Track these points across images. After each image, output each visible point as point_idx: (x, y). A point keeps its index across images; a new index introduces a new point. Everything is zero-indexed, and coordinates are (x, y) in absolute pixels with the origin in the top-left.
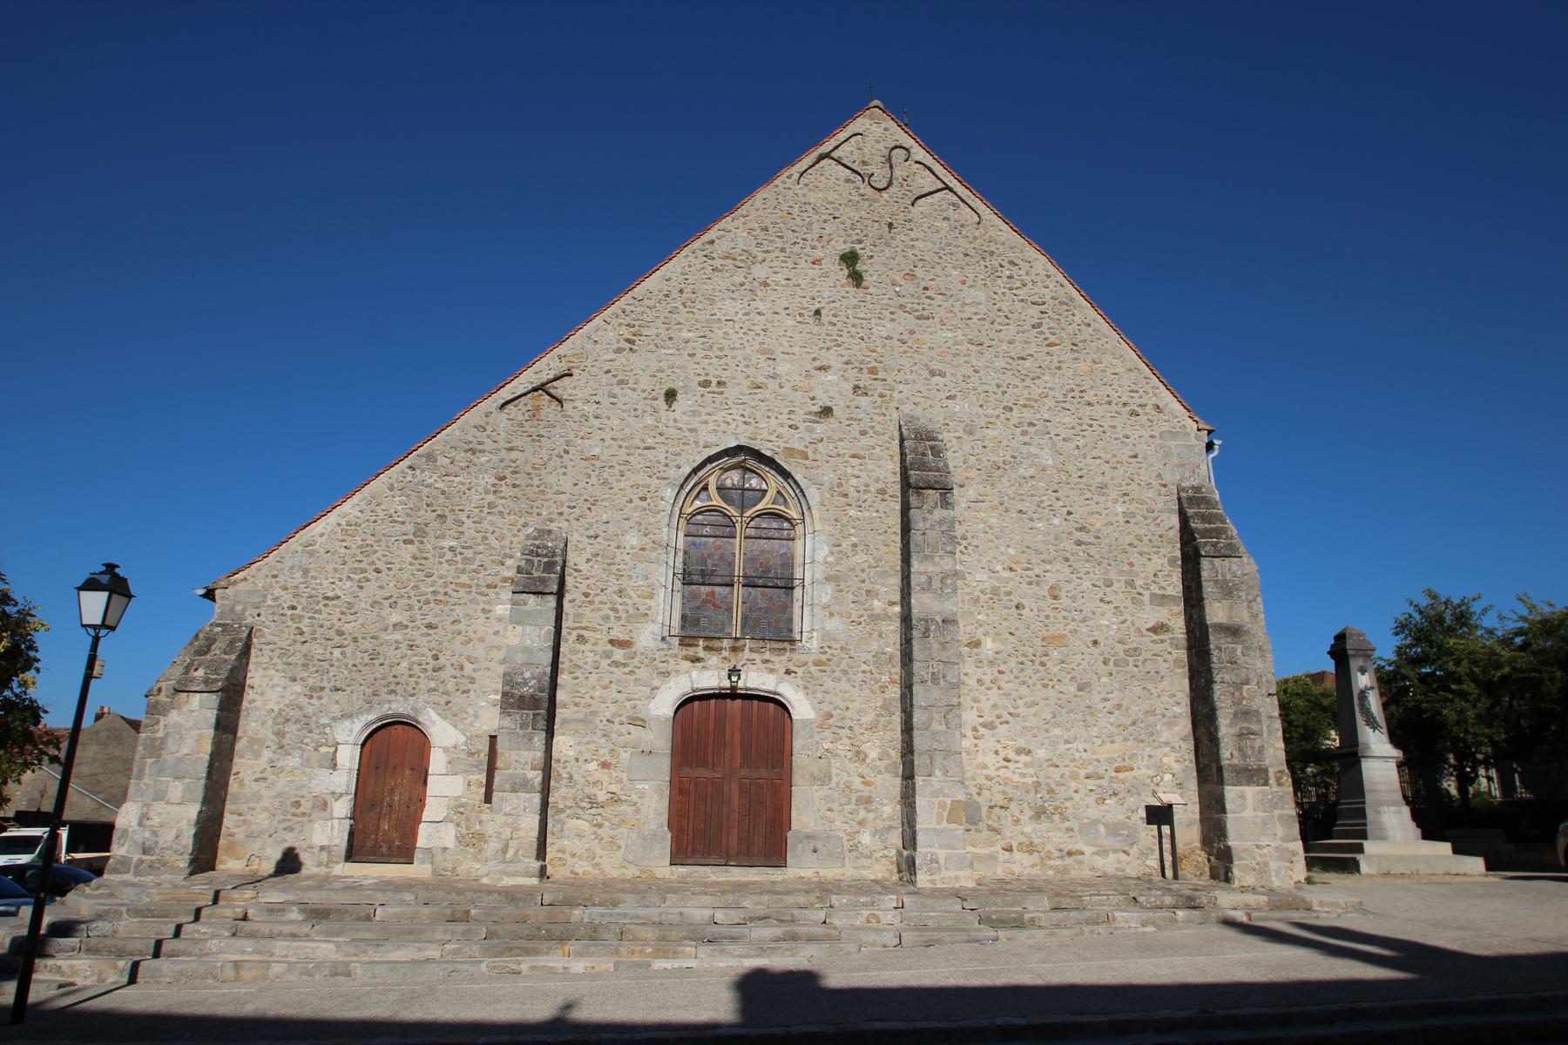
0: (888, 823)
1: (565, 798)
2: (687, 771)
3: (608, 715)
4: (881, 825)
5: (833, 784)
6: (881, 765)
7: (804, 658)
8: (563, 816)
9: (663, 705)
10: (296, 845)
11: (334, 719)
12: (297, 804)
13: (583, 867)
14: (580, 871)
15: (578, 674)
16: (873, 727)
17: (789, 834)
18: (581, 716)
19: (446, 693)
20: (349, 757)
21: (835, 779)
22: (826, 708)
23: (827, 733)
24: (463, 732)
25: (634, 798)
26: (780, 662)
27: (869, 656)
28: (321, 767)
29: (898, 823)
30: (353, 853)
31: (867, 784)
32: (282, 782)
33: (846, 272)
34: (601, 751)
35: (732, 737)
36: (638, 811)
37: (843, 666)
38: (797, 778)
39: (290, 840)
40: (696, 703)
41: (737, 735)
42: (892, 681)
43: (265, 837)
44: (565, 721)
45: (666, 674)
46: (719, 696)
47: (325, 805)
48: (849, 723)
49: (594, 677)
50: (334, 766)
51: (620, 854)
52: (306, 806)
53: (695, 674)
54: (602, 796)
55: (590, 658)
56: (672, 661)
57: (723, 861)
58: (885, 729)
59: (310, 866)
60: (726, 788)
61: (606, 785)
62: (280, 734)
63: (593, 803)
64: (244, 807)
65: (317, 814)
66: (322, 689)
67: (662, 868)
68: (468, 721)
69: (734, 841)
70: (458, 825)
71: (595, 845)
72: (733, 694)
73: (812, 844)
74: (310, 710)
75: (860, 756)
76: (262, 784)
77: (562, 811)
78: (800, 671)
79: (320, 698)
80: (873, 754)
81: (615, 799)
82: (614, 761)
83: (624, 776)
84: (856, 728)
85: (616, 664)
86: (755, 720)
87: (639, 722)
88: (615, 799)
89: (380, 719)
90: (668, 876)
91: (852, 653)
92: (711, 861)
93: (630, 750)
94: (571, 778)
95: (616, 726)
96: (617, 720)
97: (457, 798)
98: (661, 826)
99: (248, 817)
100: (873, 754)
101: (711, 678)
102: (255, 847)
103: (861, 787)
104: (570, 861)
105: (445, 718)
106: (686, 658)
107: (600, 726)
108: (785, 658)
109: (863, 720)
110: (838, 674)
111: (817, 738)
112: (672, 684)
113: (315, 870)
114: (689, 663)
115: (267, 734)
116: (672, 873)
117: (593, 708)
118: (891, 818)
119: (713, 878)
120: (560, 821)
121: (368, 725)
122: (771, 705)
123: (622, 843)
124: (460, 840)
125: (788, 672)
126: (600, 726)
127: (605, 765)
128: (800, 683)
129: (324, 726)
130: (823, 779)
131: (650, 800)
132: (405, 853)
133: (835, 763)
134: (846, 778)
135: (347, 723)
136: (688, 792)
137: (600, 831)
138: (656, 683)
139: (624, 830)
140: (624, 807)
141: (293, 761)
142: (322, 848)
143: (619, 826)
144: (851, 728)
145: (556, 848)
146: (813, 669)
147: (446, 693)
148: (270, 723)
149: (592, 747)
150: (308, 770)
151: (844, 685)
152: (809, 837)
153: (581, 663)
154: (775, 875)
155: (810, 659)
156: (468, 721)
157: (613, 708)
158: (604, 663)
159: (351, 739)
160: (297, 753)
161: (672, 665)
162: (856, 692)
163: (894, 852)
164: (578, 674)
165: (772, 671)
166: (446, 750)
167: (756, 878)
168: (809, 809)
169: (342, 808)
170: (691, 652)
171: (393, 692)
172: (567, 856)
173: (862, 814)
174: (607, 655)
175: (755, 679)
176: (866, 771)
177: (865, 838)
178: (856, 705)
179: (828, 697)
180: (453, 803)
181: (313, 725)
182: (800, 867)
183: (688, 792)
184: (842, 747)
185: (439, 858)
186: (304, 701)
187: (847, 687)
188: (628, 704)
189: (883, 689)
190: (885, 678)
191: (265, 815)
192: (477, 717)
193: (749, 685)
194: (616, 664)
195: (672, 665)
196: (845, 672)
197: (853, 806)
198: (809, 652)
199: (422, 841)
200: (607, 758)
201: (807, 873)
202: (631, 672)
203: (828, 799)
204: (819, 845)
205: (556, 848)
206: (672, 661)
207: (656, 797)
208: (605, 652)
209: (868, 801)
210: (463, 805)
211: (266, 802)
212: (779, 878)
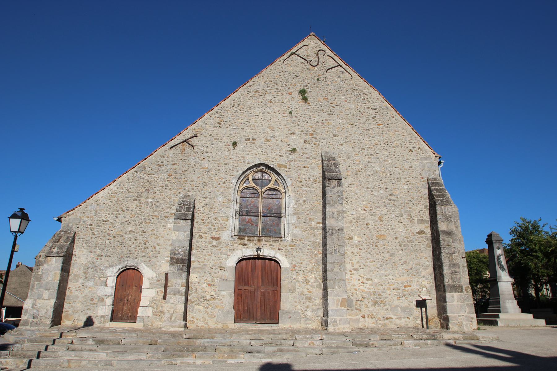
0: (317, 307)
1: (194, 298)
4: (315, 308)
5: (297, 292)
6: (315, 285)
7: (286, 244)
8: (193, 304)
9: (232, 262)
10: (92, 315)
11: (106, 267)
12: (92, 300)
13: (201, 324)
14: (200, 325)
15: (199, 250)
16: (312, 270)
17: (280, 311)
18: (200, 266)
19: (149, 257)
20: (112, 281)
22: (294, 263)
23: (294, 273)
24: (155, 272)
25: (221, 297)
26: (276, 245)
27: (310, 243)
28: (101, 285)
30: (112, 319)
31: (310, 292)
32: (86, 291)
33: (301, 97)
34: (208, 280)
36: (222, 303)
37: (300, 247)
39: (90, 313)
40: (244, 261)
41: (260, 274)
42: (319, 253)
43: (80, 312)
44: (194, 268)
45: (233, 250)
47: (103, 300)
48: (303, 269)
49: (205, 251)
50: (106, 285)
51: (215, 319)
52: (95, 300)
53: (244, 250)
54: (208, 297)
56: (235, 245)
57: (254, 322)
58: (316, 271)
59: (97, 323)
60: (256, 294)
61: (210, 292)
62: (86, 273)
63: (205, 299)
64: (72, 301)
65: (100, 303)
66: (102, 256)
67: (231, 324)
68: (157, 268)
70: (153, 308)
71: (206, 316)
72: (258, 258)
74: (97, 264)
75: (307, 281)
76: (79, 292)
77: (193, 302)
78: (284, 249)
79: (101, 259)
80: (312, 281)
81: (213, 298)
82: (213, 283)
83: (217, 289)
84: (305, 271)
85: (214, 246)
86: (267, 268)
87: (222, 268)
88: (213, 298)
89: (124, 267)
90: (233, 327)
91: (304, 242)
92: (250, 322)
93: (219, 279)
94: (196, 290)
95: (214, 270)
96: (214, 268)
97: (153, 298)
99: (73, 305)
100: (312, 281)
101: (250, 251)
102: (76, 316)
103: (307, 293)
104: (196, 321)
105: (148, 267)
106: (240, 244)
107: (208, 270)
109: (308, 267)
110: (298, 250)
111: (290, 274)
112: (235, 254)
113: (99, 325)
114: (242, 246)
115: (81, 273)
117: (205, 263)
118: (319, 305)
119: (251, 328)
120: (192, 306)
121: (119, 269)
122: (273, 262)
123: (216, 315)
124: (154, 313)
125: (279, 249)
126: (208, 270)
127: (209, 285)
128: (284, 253)
129: (103, 270)
130: (293, 290)
131: (227, 298)
132: (133, 318)
133: (297, 284)
135: (111, 269)
137: (207, 310)
138: (229, 253)
140: (217, 301)
141: (91, 283)
142: (102, 317)
143: (215, 308)
144: (303, 271)
145: (191, 316)
146: (289, 248)
147: (149, 257)
148: (82, 268)
149: (204, 278)
150: (96, 287)
151: (301, 254)
153: (200, 246)
154: (274, 327)
155: (288, 244)
156: (157, 268)
158: (209, 246)
159: (113, 275)
160: (92, 280)
162: (305, 257)
163: (320, 318)
164: (199, 250)
165: (273, 249)
166: (149, 279)
167: (267, 328)
168: (287, 301)
169: (109, 301)
170: (242, 241)
171: (129, 257)
172: (195, 320)
173: (308, 303)
174: (210, 243)
175: (267, 252)
176: (309, 287)
177: (309, 313)
178: (305, 262)
179: (295, 259)
180: (151, 299)
181: (98, 270)
182: (284, 324)
183: (241, 295)
184: (300, 278)
185: (146, 320)
186: (95, 260)
187: (302, 255)
188: (218, 261)
189: (316, 256)
190: (316, 252)
191: (80, 304)
192: (161, 266)
193: (265, 254)
194: (214, 246)
196: (301, 249)
197: (304, 300)
199: (139, 314)
200: (210, 282)
202: (220, 249)
204: (291, 316)
205: (191, 316)
206: (235, 245)
207: (229, 297)
209: (310, 298)
210: (155, 300)
211: (80, 299)
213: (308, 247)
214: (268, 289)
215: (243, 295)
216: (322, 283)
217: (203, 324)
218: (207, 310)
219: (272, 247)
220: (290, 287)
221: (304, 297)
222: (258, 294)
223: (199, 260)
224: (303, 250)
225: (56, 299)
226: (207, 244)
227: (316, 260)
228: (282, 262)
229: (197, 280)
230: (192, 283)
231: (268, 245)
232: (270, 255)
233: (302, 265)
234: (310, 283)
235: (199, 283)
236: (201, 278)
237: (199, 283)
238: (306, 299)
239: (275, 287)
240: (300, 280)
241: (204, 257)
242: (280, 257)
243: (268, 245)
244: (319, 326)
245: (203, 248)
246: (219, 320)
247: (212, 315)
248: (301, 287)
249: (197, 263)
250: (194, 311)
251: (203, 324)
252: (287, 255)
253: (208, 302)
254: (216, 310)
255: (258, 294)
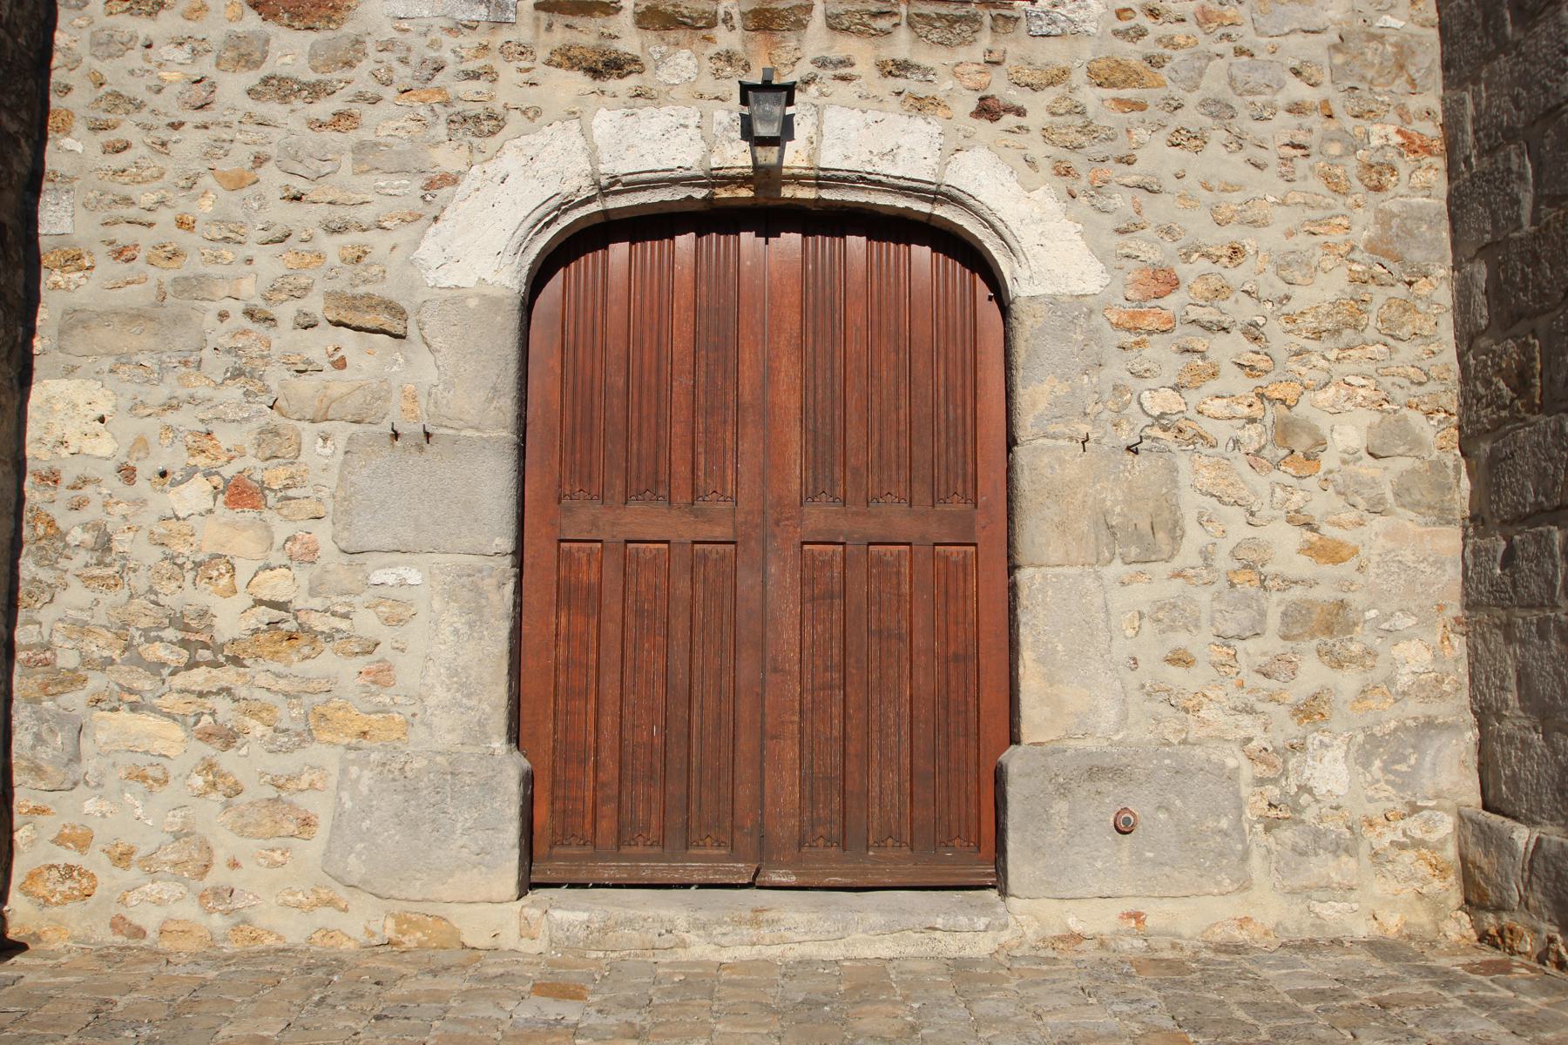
0: (1414, 709)
1: (83, 629)
2: (583, 518)
3: (250, 290)
4: (1389, 715)
5: (1188, 555)
6: (1384, 475)
7: (1053, 53)
8: (76, 700)
9: (478, 247)
13: (162, 906)
14: (149, 919)
15: (127, 130)
16: (1342, 325)
17: (1014, 760)
18: (138, 296)
21: (1195, 537)
22: (1150, 249)
23: (1160, 352)
25: (367, 623)
26: (954, 68)
27: (1314, 49)
29: (1456, 707)
31: (1329, 553)
34: (226, 437)
35: (768, 377)
36: (381, 677)
37: (1214, 83)
38: (1039, 533)
40: (619, 251)
41: (788, 371)
42: (1412, 146)
44: (76, 320)
45: (483, 124)
46: (713, 215)
48: (1247, 311)
49: (190, 142)
51: (312, 849)
53: (604, 122)
54: (232, 619)
55: (176, 68)
56: (509, 73)
57: (743, 870)
58: (1391, 335)
60: (747, 581)
61: (254, 565)
63: (197, 642)
67: (487, 906)
69: (785, 787)
71: (211, 816)
72: (763, 207)
73: (1111, 799)
75: (1293, 443)
77: (73, 680)
78: (1037, 106)
80: (1348, 435)
81: (286, 630)
82: (276, 476)
83: (322, 534)
84: (1274, 329)
85: (280, 88)
86: (857, 314)
87: (382, 320)
88: (286, 630)
90: (509, 939)
91: (1247, 38)
92: (696, 870)
93: (342, 432)
94: (104, 545)
95: (285, 337)
96: (286, 312)
98: (478, 734)
100: (1348, 435)
101: (675, 133)
103: (1304, 566)
104: (109, 878)
106: (567, 59)
107: (220, 335)
108: (977, 53)
109: (1303, 298)
110: (1190, 117)
111: (1117, 369)
112: (510, 161)
114: (579, 81)
116: (527, 931)
117: (193, 265)
118: (1431, 689)
119: (700, 949)
120: (62, 719)
122: (922, 254)
123: (318, 805)
125: (987, 110)
126: (220, 335)
127: (241, 493)
128: (1039, 150)
130: (1149, 535)
131: (436, 634)
133: (1195, 472)
134: (1239, 530)
136: (593, 598)
137: (228, 761)
138: (447, 158)
139: (324, 754)
140: (327, 662)
143: (306, 736)
144: (1254, 333)
145: (50, 825)
146: (1090, 96)
149: (186, 419)
151: (1218, 160)
152: (1097, 771)
153: (135, 88)
154: (958, 928)
155: (1076, 56)
157: (271, 264)
158: (233, 86)
161: (508, 88)
162: (1268, 187)
163: (1446, 826)
164: (127, 130)
165: (921, 105)
167: (885, 948)
168: (1091, 658)
170: (586, 33)
172: (95, 861)
173: (1312, 674)
174: (244, 54)
175: (850, 136)
176: (1320, 504)
177: (1330, 772)
178: (1271, 238)
179: (1158, 209)
182: (1065, 896)
183: (593, 598)
184: (1221, 405)
187: (1233, 166)
188: (331, 246)
189: (1377, 177)
190: (1383, 133)
193: (832, 159)
194: (280, 88)
195: (508, 88)
196: (1219, 110)
197: (1271, 643)
198: (1074, 33)
200: (251, 464)
201: (1093, 918)
202: (343, 120)
203: (1168, 615)
204: (1141, 806)
205: (50, 825)
206: (509, 73)
207: (453, 618)
208: (234, 41)
209: (1334, 621)
212: (982, 946)
213: (1298, 90)
214: (873, 529)
215: (612, 605)
216: (1453, 456)
217: (189, 910)
218: (228, 761)
219: (911, 84)
220: (1112, 498)
221: (1274, 605)
222: (775, 587)
223: (123, 234)
224: (1244, 123)
225: (1457, 69)
226: (206, 66)
227: (1384, 218)
228: (1027, 238)
229: (104, 446)
230: (52, 478)
231: (864, 67)
232: (885, 169)
233: (1236, 275)
234: (1329, 460)
235: (128, 473)
236: (151, 427)
237: (128, 473)
238: (1298, 622)
239: (957, 506)
240: (1221, 432)
241: (182, 204)
242: (996, 187)
243: (864, 67)
244: (1436, 906)
245: (170, 106)
246: (355, 867)
247: (283, 813)
248: (1231, 507)
249: (107, 268)
250: (90, 766)
251: (189, 910)
252: (1079, 166)
253: (228, 676)
254: (315, 752)
255: (775, 587)
